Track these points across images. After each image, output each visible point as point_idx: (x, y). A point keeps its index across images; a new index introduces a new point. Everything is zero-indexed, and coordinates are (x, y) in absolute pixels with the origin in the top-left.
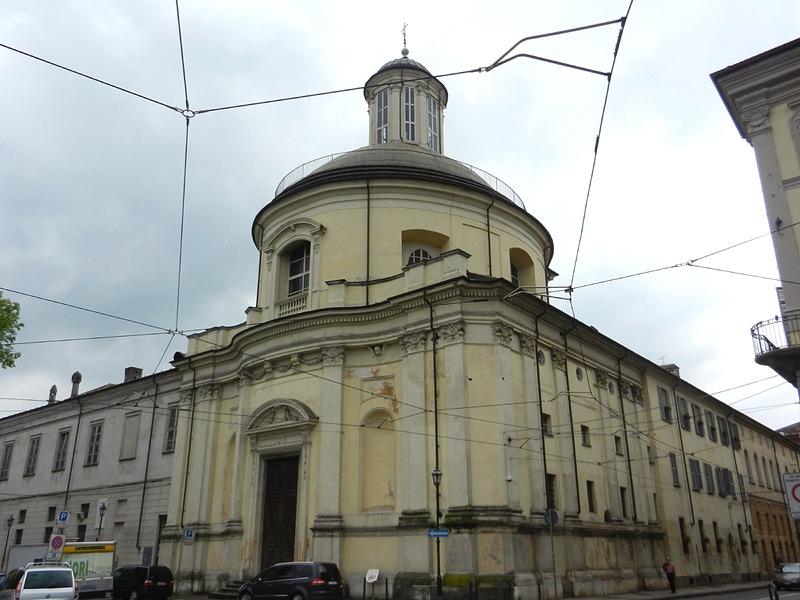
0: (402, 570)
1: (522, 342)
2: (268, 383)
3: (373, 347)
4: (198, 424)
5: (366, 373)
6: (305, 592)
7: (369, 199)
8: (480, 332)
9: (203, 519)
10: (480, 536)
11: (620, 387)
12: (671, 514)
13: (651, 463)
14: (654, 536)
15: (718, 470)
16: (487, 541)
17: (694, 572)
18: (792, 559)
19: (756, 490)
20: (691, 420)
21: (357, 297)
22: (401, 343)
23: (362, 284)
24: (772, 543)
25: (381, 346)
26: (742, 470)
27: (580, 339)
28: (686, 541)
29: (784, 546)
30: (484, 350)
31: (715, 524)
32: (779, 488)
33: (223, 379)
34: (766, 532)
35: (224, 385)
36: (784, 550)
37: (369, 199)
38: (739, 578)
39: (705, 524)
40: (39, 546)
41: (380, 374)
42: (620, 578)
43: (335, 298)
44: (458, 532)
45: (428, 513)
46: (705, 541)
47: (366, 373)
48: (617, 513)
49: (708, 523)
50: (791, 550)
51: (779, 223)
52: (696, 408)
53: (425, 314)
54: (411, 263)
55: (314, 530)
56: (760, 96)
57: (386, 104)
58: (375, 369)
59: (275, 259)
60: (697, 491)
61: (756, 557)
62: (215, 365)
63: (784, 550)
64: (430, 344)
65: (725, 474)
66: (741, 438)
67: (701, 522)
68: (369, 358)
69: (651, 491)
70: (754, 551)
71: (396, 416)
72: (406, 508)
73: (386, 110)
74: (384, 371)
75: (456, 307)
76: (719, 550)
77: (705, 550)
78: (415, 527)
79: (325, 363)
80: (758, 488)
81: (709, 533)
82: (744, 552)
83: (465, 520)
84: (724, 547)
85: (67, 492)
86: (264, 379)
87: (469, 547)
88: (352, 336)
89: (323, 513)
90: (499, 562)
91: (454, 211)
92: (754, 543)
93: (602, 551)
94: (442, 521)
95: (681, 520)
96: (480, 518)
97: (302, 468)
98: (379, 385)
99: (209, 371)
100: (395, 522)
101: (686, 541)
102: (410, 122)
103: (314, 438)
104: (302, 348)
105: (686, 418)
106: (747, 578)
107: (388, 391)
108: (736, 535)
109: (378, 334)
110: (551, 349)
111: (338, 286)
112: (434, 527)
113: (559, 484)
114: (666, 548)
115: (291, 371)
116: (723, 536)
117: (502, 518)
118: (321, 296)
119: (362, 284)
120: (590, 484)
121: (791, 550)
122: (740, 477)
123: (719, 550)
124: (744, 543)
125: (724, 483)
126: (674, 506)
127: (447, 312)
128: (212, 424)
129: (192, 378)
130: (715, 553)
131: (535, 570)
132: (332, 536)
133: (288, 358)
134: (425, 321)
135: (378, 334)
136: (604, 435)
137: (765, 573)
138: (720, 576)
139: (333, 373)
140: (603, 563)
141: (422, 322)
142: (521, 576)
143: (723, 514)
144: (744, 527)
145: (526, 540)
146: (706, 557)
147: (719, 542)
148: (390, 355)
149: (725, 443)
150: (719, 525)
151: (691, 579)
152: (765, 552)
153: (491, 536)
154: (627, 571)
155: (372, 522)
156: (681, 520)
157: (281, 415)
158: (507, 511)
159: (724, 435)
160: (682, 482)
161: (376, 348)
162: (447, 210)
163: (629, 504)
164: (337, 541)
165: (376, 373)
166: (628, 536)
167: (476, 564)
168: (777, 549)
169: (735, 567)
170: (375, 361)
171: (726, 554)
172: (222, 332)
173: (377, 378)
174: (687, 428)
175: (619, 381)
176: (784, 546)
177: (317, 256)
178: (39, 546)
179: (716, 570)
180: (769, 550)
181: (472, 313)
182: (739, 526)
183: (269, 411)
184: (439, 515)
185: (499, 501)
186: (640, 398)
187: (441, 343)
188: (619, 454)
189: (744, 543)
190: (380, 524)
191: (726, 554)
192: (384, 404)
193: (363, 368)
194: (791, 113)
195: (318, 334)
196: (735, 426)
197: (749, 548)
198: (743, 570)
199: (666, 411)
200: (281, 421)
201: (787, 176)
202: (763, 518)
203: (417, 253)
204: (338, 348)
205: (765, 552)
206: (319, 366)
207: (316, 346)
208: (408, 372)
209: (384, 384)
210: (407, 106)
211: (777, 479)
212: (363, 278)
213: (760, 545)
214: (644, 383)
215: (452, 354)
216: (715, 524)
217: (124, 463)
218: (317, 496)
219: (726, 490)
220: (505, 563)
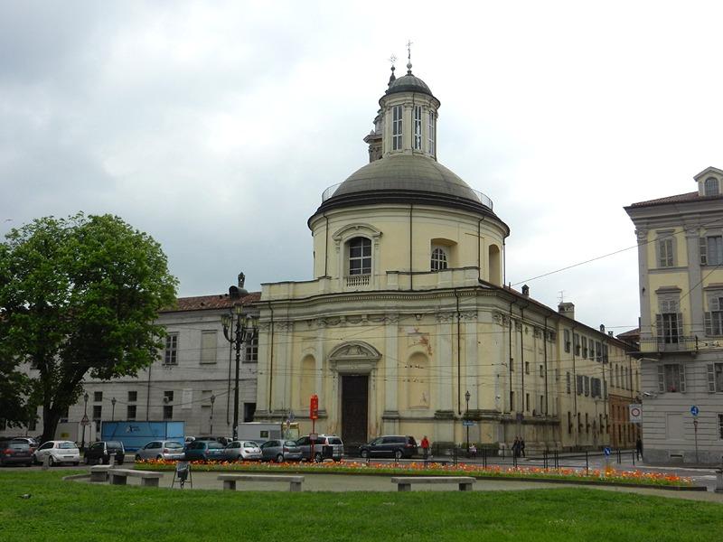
0: (436, 440)
1: (504, 319)
2: (343, 329)
4: (277, 348)
5: (410, 330)
6: (402, 449)
7: (411, 217)
8: (486, 316)
9: (287, 407)
10: (482, 425)
11: (545, 334)
12: (564, 411)
13: (557, 379)
14: (555, 424)
15: (592, 379)
16: (486, 427)
17: (572, 444)
18: (636, 426)
19: (615, 391)
20: (581, 349)
21: (404, 283)
22: (438, 315)
23: (407, 273)
24: (619, 426)
25: (421, 315)
26: (608, 380)
27: (531, 311)
28: (570, 426)
29: (627, 428)
30: (487, 326)
31: (587, 415)
32: (629, 388)
33: (296, 318)
34: (616, 418)
35: (295, 322)
36: (627, 431)
37: (411, 217)
38: (597, 448)
39: (581, 414)
40: (160, 422)
42: (538, 447)
43: (393, 283)
45: (453, 412)
46: (580, 425)
47: (410, 330)
48: (538, 412)
49: (583, 414)
50: (631, 431)
51: (644, 290)
52: (584, 338)
53: (453, 301)
55: (383, 418)
56: (644, 223)
57: (400, 117)
59: (342, 245)
60: (579, 395)
61: (608, 435)
62: (289, 308)
63: (627, 431)
64: (456, 320)
65: (596, 381)
66: (609, 355)
67: (579, 414)
68: (412, 321)
69: (555, 397)
70: (608, 432)
71: (430, 357)
72: (439, 408)
73: (400, 122)
74: (422, 330)
75: (473, 301)
76: (587, 431)
77: (580, 431)
78: (446, 419)
79: (387, 323)
80: (615, 389)
81: (583, 421)
82: (602, 431)
83: (474, 417)
84: (590, 429)
85: (149, 382)
86: (338, 325)
87: (478, 429)
88: (403, 308)
89: (387, 409)
91: (461, 225)
92: (608, 426)
93: (531, 432)
94: (462, 416)
95: (569, 413)
97: (371, 384)
98: (419, 338)
99: (285, 312)
100: (432, 415)
101: (570, 426)
103: (380, 365)
104: (370, 312)
105: (578, 347)
106: (602, 448)
107: (425, 342)
108: (598, 422)
109: (421, 308)
110: (515, 320)
111: (393, 275)
112: (456, 419)
113: (515, 396)
114: (560, 430)
115: (360, 324)
116: (590, 422)
117: (493, 416)
118: (377, 282)
119: (407, 273)
121: (631, 431)
122: (605, 382)
123: (587, 431)
124: (602, 427)
125: (594, 388)
126: (567, 404)
127: (468, 302)
128: (290, 345)
129: (270, 314)
130: (585, 433)
131: (554, 441)
133: (360, 316)
135: (421, 308)
136: (411, 273)
137: (612, 446)
138: (586, 447)
139: (391, 330)
140: (531, 439)
141: (450, 306)
142: (501, 445)
143: (591, 408)
144: (603, 416)
145: (502, 426)
146: (579, 436)
147: (588, 426)
148: (426, 320)
149: (599, 360)
150: (589, 415)
151: (571, 448)
152: (614, 432)
153: (487, 425)
154: (541, 443)
155: (415, 415)
156: (569, 413)
157: (354, 351)
158: (496, 412)
159: (599, 354)
160: (572, 390)
162: (456, 224)
163: (544, 405)
164: (397, 424)
165: (417, 330)
166: (543, 423)
167: (480, 438)
168: (622, 430)
169: (595, 442)
170: (417, 323)
171: (591, 434)
172: (292, 285)
173: (417, 333)
174: (578, 354)
175: (545, 331)
176: (627, 428)
177: (377, 252)
178: (160, 422)
179: (584, 444)
180: (617, 431)
181: (483, 305)
182: (601, 415)
183: (347, 347)
184: (460, 413)
185: (491, 407)
186: (554, 339)
187: (462, 320)
188: (542, 376)
189: (602, 427)
190: (420, 416)
191: (591, 434)
192: (422, 349)
193: (410, 326)
194: (656, 236)
195: (382, 304)
196: (606, 347)
197: (605, 430)
198: (600, 444)
199: (568, 344)
200: (354, 354)
201: (650, 268)
202: (616, 409)
203: (437, 250)
204: (395, 314)
205: (614, 432)
206: (381, 323)
207: (380, 311)
208: (441, 335)
211: (629, 382)
212: (408, 270)
213: (612, 427)
214: (557, 329)
215: (470, 327)
216: (587, 415)
217: (205, 366)
218: (382, 398)
219: (596, 393)
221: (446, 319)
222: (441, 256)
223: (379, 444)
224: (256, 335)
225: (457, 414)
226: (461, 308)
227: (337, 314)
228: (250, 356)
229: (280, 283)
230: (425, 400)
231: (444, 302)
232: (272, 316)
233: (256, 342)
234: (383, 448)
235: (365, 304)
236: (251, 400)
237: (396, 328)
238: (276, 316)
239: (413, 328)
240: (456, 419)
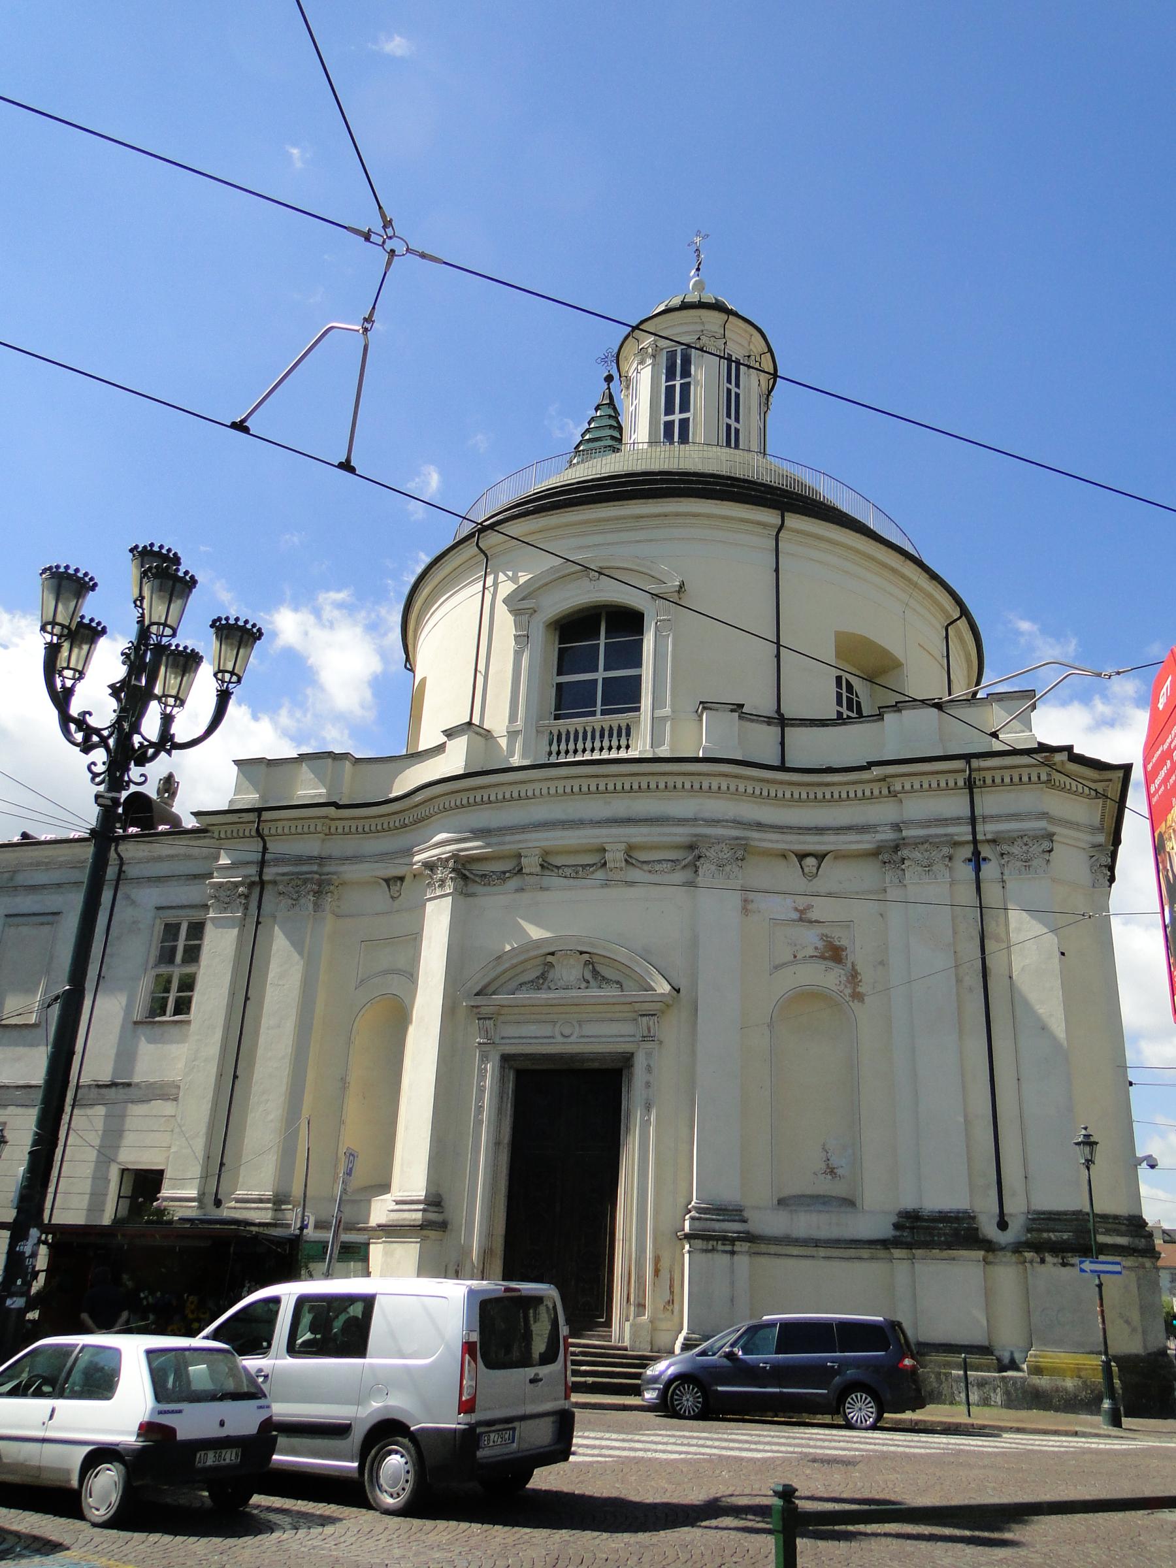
3: (802, 856)
25: (821, 857)
41: (814, 915)
44: (1064, 1265)
47: (782, 908)
54: (180, 923)
58: (802, 902)
72: (908, 1203)
90: (1134, 1330)
96: (1102, 1239)
100: (883, 1228)
102: (732, 422)
109: (820, 830)
112: (988, 1246)
119: (769, 721)
120: (180, 1412)
132: (733, 1253)
134: (956, 821)
161: (810, 862)
164: (743, 1262)
165: (802, 912)
173: (803, 918)
184: (1003, 1225)
209: (824, 937)
210: (729, 391)
220: (1144, 1332)
221: (928, 867)
222: (850, 700)
223: (765, 1358)
224: (197, 929)
225: (989, 1229)
226: (986, 830)
227: (511, 843)
228: (165, 1000)
229: (374, 308)
230: (831, 1171)
231: (919, 807)
232: (262, 864)
233: (192, 954)
234: (779, 1374)
235: (620, 806)
236: (147, 1160)
237: (736, 899)
238: (278, 861)
239: (789, 901)
240: (988, 1246)
